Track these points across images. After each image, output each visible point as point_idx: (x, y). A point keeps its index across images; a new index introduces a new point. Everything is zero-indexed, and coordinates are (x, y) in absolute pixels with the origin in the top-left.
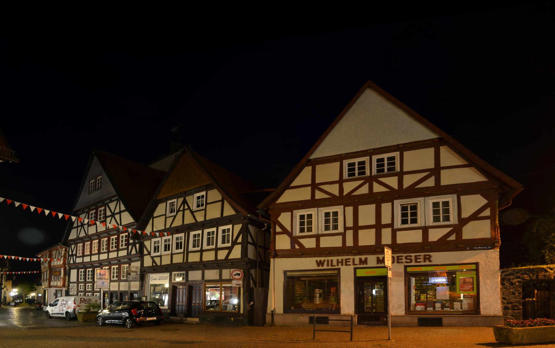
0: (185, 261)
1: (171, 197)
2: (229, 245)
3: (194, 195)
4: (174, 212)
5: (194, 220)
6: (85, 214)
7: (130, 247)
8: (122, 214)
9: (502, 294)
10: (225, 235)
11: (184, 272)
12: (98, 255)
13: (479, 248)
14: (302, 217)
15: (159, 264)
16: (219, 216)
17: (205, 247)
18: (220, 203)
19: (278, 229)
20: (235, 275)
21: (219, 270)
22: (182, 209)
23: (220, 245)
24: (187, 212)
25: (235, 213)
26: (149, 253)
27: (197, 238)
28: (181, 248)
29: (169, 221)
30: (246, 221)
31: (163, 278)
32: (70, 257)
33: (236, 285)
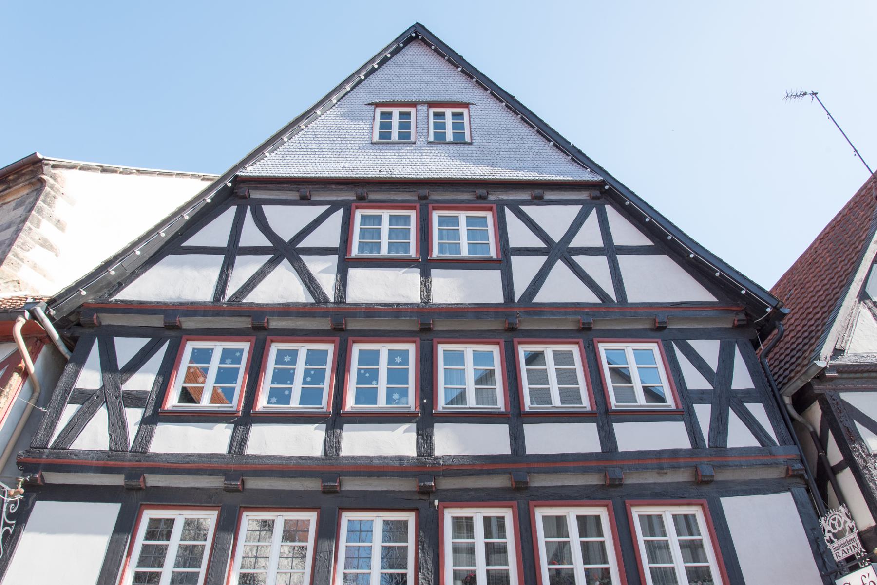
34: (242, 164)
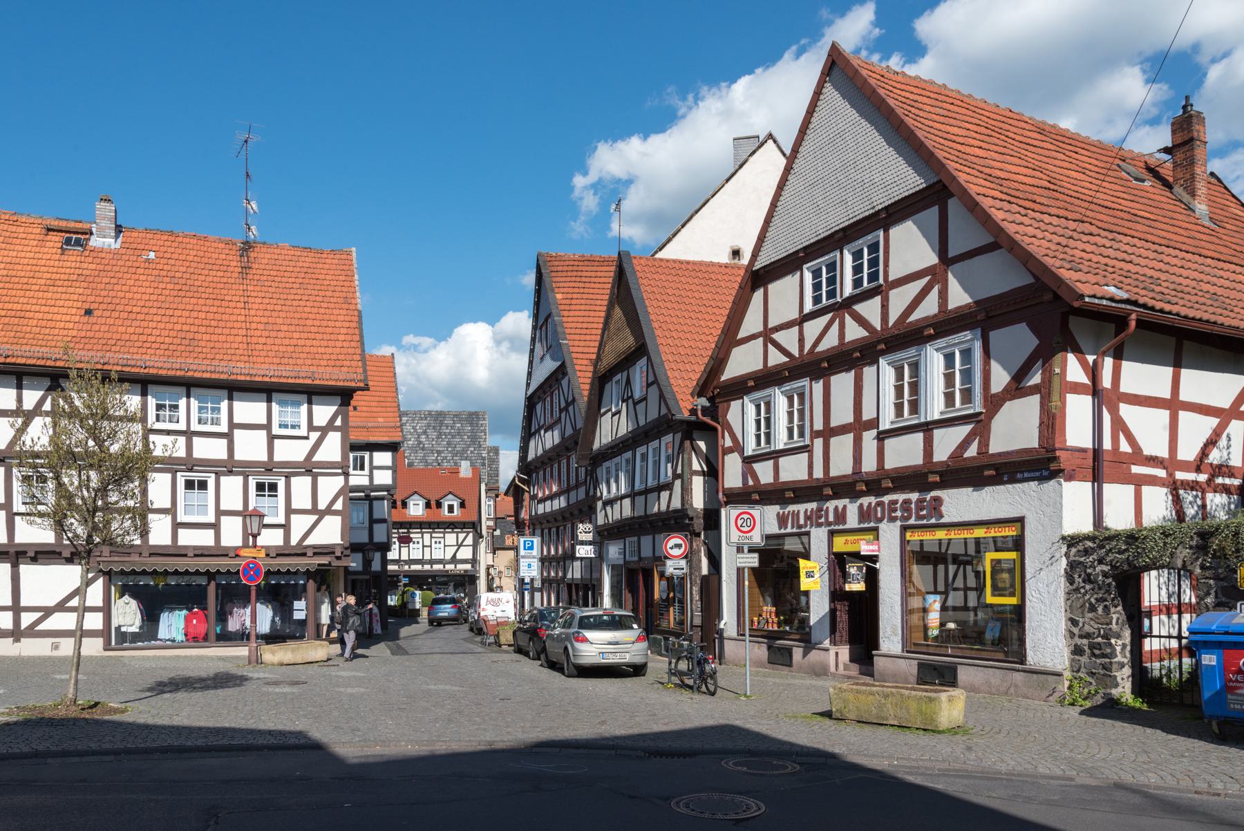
2: (977, 406)
9: (1068, 609)
13: (1026, 475)
14: (280, 426)
20: (671, 548)
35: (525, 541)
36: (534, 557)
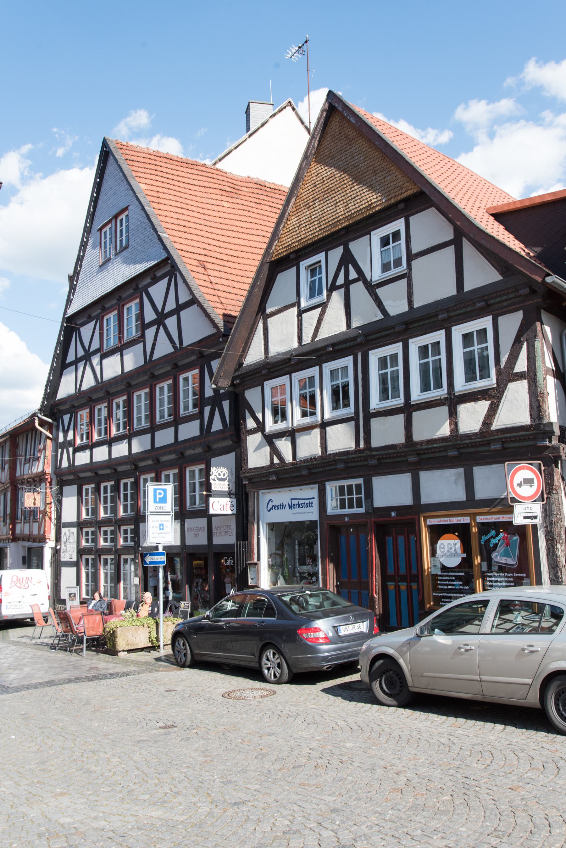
0: (362, 445)
1: (310, 249)
2: (492, 381)
3: (372, 233)
4: (320, 293)
5: (379, 312)
6: (94, 322)
7: (207, 410)
8: (183, 313)
10: (387, 373)
11: (360, 481)
12: (172, 429)
15: (288, 458)
16: (453, 291)
17: (416, 395)
18: (450, 251)
19: (251, 424)
20: (520, 485)
21: (461, 470)
22: (341, 280)
23: (416, 395)
24: (357, 290)
25: (501, 278)
26: (261, 427)
27: (391, 367)
28: (347, 405)
29: (310, 318)
30: (537, 300)
31: (301, 502)
32: (60, 451)
33: (525, 518)
34: (65, 312)
35: (155, 490)
36: (167, 514)
